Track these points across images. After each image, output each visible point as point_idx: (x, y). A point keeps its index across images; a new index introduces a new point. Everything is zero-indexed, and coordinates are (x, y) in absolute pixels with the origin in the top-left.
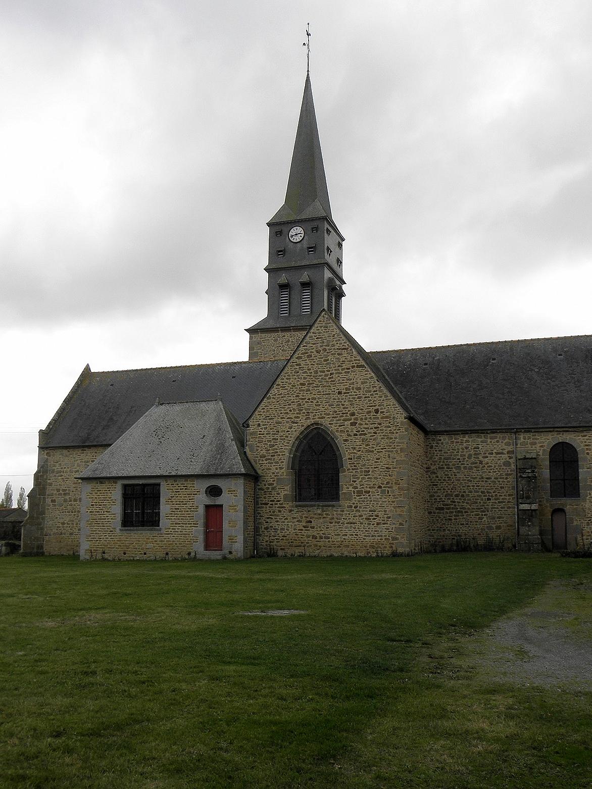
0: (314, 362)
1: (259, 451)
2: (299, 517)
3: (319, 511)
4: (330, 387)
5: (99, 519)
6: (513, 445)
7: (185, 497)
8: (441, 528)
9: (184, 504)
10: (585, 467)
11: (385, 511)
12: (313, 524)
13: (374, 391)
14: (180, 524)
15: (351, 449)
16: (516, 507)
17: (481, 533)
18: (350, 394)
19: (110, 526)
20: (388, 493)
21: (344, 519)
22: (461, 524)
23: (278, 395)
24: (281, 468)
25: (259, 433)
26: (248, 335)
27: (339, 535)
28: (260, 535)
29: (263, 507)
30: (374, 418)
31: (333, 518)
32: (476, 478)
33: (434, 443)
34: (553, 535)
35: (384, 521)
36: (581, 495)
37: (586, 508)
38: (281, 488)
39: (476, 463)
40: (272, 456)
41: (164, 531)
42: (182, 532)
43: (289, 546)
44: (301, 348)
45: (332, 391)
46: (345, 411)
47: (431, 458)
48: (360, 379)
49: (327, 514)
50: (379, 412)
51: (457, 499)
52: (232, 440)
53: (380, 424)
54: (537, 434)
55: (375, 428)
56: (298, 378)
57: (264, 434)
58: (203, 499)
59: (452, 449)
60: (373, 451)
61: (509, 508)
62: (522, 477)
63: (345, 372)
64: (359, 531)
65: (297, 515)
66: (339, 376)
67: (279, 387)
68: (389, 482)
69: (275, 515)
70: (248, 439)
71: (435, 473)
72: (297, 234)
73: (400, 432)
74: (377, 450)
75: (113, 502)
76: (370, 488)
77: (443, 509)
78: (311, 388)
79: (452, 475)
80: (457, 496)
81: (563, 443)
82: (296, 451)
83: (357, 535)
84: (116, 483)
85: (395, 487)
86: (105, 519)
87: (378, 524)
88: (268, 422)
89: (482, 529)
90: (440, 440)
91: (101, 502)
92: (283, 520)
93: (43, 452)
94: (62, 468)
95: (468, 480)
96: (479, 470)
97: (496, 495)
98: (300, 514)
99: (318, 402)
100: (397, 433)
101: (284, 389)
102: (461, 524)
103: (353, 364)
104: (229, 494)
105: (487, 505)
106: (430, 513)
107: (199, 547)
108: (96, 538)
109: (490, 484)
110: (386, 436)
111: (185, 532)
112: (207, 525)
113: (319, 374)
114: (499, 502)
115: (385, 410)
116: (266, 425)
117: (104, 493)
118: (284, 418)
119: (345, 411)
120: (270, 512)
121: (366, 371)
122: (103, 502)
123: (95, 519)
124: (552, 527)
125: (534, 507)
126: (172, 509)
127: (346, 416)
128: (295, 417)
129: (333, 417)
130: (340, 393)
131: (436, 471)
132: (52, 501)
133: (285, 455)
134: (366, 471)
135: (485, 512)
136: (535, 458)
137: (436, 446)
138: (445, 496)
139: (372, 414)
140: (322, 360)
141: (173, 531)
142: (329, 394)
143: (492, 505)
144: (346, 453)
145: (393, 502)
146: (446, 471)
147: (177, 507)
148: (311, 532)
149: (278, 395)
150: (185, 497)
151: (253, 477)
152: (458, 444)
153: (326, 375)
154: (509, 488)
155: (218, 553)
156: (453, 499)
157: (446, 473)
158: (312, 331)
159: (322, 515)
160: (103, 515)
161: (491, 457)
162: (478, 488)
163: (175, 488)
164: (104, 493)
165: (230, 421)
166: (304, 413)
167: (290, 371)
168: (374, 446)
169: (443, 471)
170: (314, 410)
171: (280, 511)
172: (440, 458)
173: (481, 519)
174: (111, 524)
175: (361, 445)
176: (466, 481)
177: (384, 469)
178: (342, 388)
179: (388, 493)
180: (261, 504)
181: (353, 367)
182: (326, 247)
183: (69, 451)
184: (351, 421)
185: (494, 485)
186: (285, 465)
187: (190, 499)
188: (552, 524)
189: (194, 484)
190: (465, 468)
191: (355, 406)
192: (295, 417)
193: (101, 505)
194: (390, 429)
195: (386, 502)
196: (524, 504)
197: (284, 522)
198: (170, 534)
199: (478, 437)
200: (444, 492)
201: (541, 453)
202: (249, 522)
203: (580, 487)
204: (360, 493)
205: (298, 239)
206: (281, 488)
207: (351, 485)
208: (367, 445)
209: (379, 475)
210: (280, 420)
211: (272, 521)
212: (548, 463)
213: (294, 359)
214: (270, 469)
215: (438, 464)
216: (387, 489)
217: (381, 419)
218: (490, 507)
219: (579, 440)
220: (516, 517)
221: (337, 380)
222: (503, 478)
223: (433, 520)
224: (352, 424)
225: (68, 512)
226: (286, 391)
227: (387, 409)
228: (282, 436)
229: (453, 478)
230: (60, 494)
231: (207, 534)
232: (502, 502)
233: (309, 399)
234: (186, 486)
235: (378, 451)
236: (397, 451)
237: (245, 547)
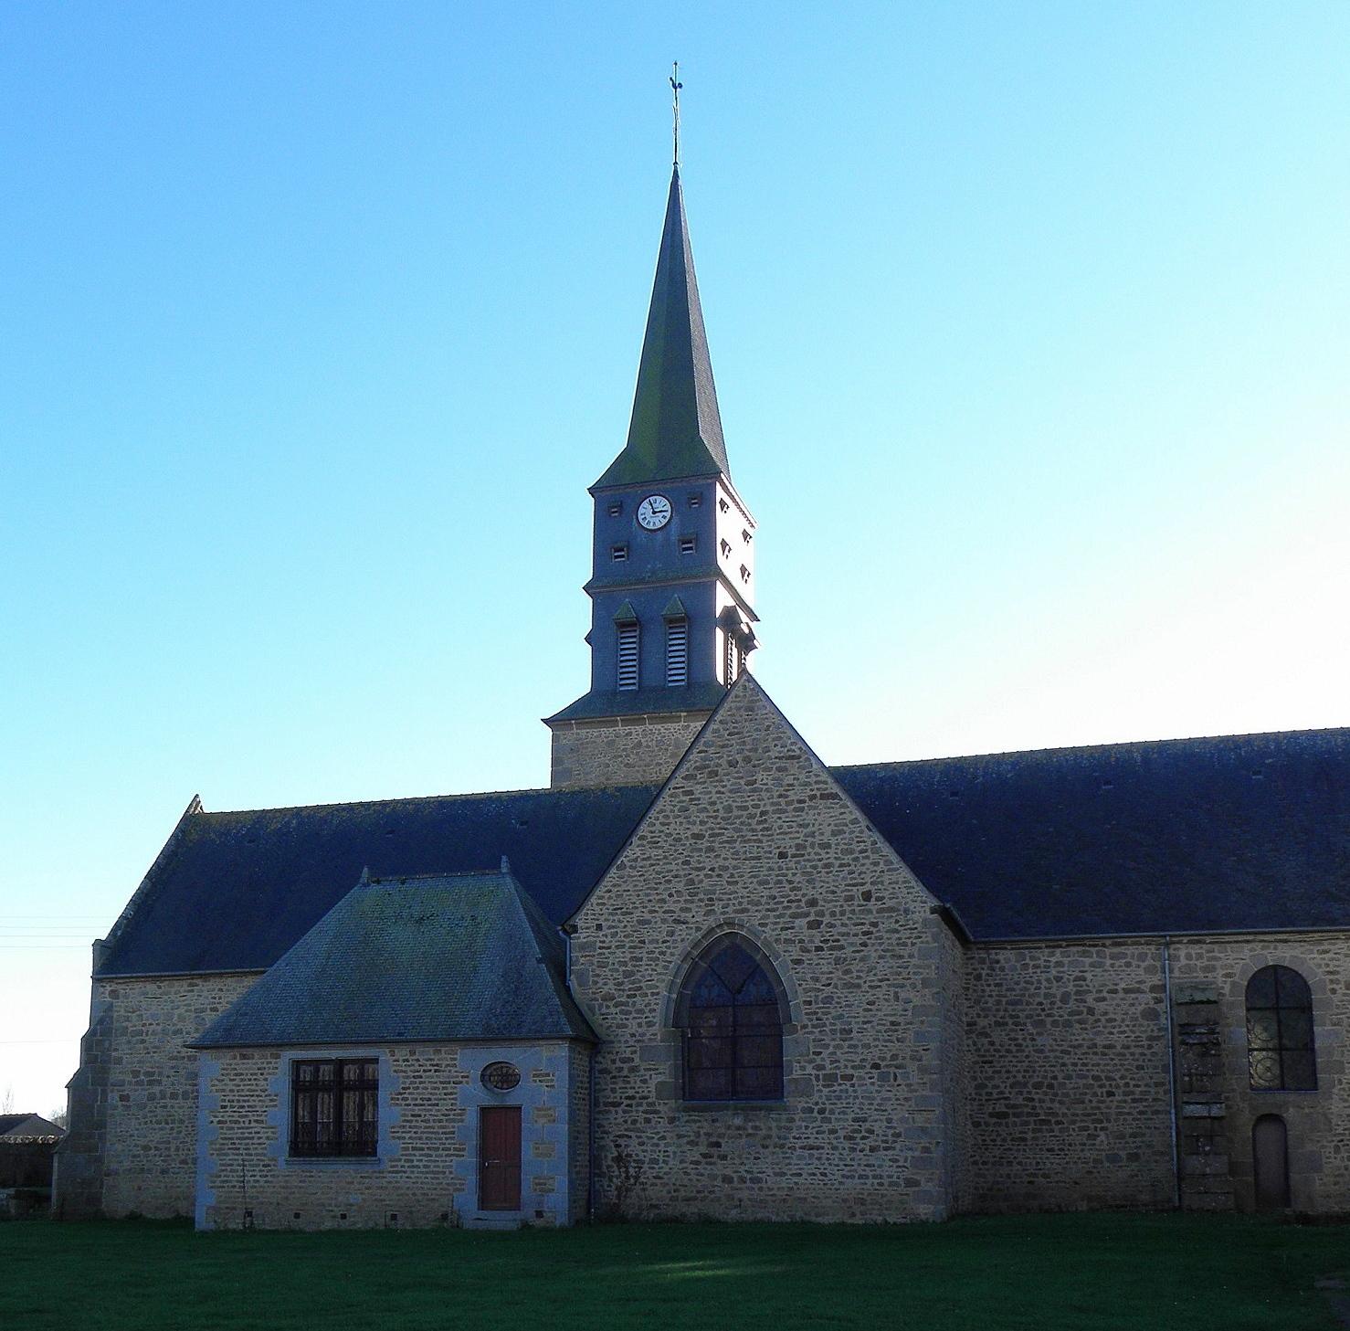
0: (724, 787)
1: (599, 985)
2: (692, 1134)
3: (738, 1121)
4: (761, 842)
5: (238, 1139)
6: (1165, 972)
7: (435, 1089)
8: (1002, 1158)
9: (434, 1105)
10: (1328, 1022)
11: (889, 1121)
12: (724, 1149)
13: (861, 852)
14: (422, 1149)
15: (810, 982)
16: (1173, 1111)
17: (1095, 1170)
18: (807, 857)
19: (265, 1155)
20: (895, 1080)
21: (794, 1138)
22: (1048, 1150)
23: (644, 859)
24: (650, 1024)
25: (599, 944)
26: (548, 732)
27: (785, 1174)
28: (601, 1175)
29: (610, 1111)
30: (862, 912)
31: (769, 1137)
32: (1080, 1046)
33: (983, 969)
34: (1256, 1174)
35: (886, 1142)
36: (1320, 1083)
37: (1332, 1113)
38: (650, 1069)
39: (1080, 1013)
40: (628, 996)
41: (387, 1165)
42: (429, 1167)
43: (670, 1200)
44: (694, 756)
45: (765, 852)
46: (796, 895)
47: (977, 1002)
48: (829, 825)
49: (756, 1128)
50: (873, 899)
51: (1038, 1093)
52: (539, 961)
53: (875, 925)
54: (1216, 947)
55: (865, 933)
56: (689, 823)
57: (609, 948)
58: (476, 1095)
59: (1025, 982)
60: (859, 986)
61: (1157, 1112)
62: (1187, 1044)
63: (796, 810)
64: (830, 1164)
65: (688, 1129)
66: (780, 818)
67: (645, 842)
68: (897, 1055)
69: (638, 1130)
70: (574, 959)
71: (987, 1035)
72: (655, 513)
73: (922, 942)
74: (868, 984)
75: (271, 1100)
76: (853, 1067)
77: (1005, 1115)
78: (716, 845)
79: (1024, 1039)
80: (1038, 1086)
81: (1275, 967)
82: (684, 985)
83: (825, 1175)
84: (278, 1057)
85: (912, 1067)
86: (253, 1138)
87: (872, 1149)
88: (620, 921)
89: (1095, 1161)
90: (998, 962)
91: (244, 1101)
92: (655, 1141)
93: (102, 989)
94: (144, 1025)
95: (1062, 1052)
96: (1086, 1029)
97: (1127, 1085)
98: (695, 1126)
99: (732, 876)
100: (913, 944)
101: (656, 848)
102: (1048, 1150)
103: (812, 790)
104: (536, 1081)
105: (1107, 1108)
106: (976, 1125)
107: (467, 1201)
108: (231, 1181)
109: (1112, 1059)
110: (887, 951)
111: (435, 1167)
112: (484, 1152)
113: (736, 813)
114: (1134, 1101)
115: (886, 894)
116: (614, 927)
117: (250, 1080)
118: (657, 912)
119: (796, 895)
120: (626, 1122)
121: (842, 807)
122: (248, 1101)
123: (230, 1139)
124: (1255, 1156)
125: (1215, 1111)
126: (405, 1115)
127: (798, 907)
128: (682, 910)
129: (768, 910)
130: (782, 855)
131: (988, 1030)
132: (122, 1098)
133: (658, 994)
134: (844, 1029)
135: (1102, 1122)
136: (1215, 1002)
137: (988, 974)
138: (1011, 1087)
139: (856, 903)
140: (742, 782)
141: (407, 1164)
142: (759, 858)
143: (1117, 1107)
144: (800, 990)
145: (906, 1099)
146: (1012, 1030)
147: (416, 1112)
148: (720, 1169)
149: (644, 859)
150: (435, 1089)
151: (589, 1041)
152: (1039, 971)
153: (751, 816)
154: (1156, 1068)
155: (511, 1215)
156: (1029, 1093)
157: (1013, 1035)
158: (718, 717)
159: (745, 1129)
160: (248, 1128)
161: (1113, 999)
162: (1085, 1068)
163: (412, 1068)
164: (250, 1080)
165: (527, 915)
166: (701, 900)
167: (668, 808)
168: (861, 974)
169: (1005, 1030)
170: (726, 893)
171: (648, 1121)
172: (999, 1003)
173: (1092, 1137)
174: (265, 1148)
175: (831, 973)
176: (1058, 1054)
177: (884, 1025)
178: (788, 844)
179: (895, 1080)
180: (606, 1104)
181: (813, 797)
182: (719, 541)
183: (160, 987)
184: (808, 919)
185: (1122, 1062)
186: (658, 1018)
187: (445, 1094)
188: (1254, 1149)
189: (455, 1059)
190: (1055, 1023)
191: (818, 885)
192: (682, 910)
193: (243, 1107)
194: (897, 936)
195: (890, 1099)
196: (1192, 1103)
197: (657, 1145)
198: (401, 1172)
199: (1085, 954)
200: (1008, 1078)
201: (1227, 990)
202: (580, 1144)
203: (1318, 1066)
204: (831, 1079)
205: (659, 522)
206: (650, 1069)
207: (810, 1062)
208: (847, 972)
209: (875, 1040)
210: (647, 916)
211: (629, 1141)
212: (1243, 1012)
213: (678, 781)
214: (626, 1026)
215: (995, 1016)
216: (892, 1070)
217: (878, 913)
218: (1113, 1111)
219: (1312, 961)
220: (1174, 1134)
221: (775, 826)
222: (1142, 1046)
223: (984, 1140)
224: (811, 925)
225: (158, 1122)
226: (661, 851)
227: (891, 891)
228: (653, 952)
229: (1027, 1046)
230: (139, 1083)
231: (483, 1171)
232: (1141, 1100)
233: (712, 870)
234: (437, 1065)
235: (873, 984)
236: (914, 986)
237: (573, 1202)
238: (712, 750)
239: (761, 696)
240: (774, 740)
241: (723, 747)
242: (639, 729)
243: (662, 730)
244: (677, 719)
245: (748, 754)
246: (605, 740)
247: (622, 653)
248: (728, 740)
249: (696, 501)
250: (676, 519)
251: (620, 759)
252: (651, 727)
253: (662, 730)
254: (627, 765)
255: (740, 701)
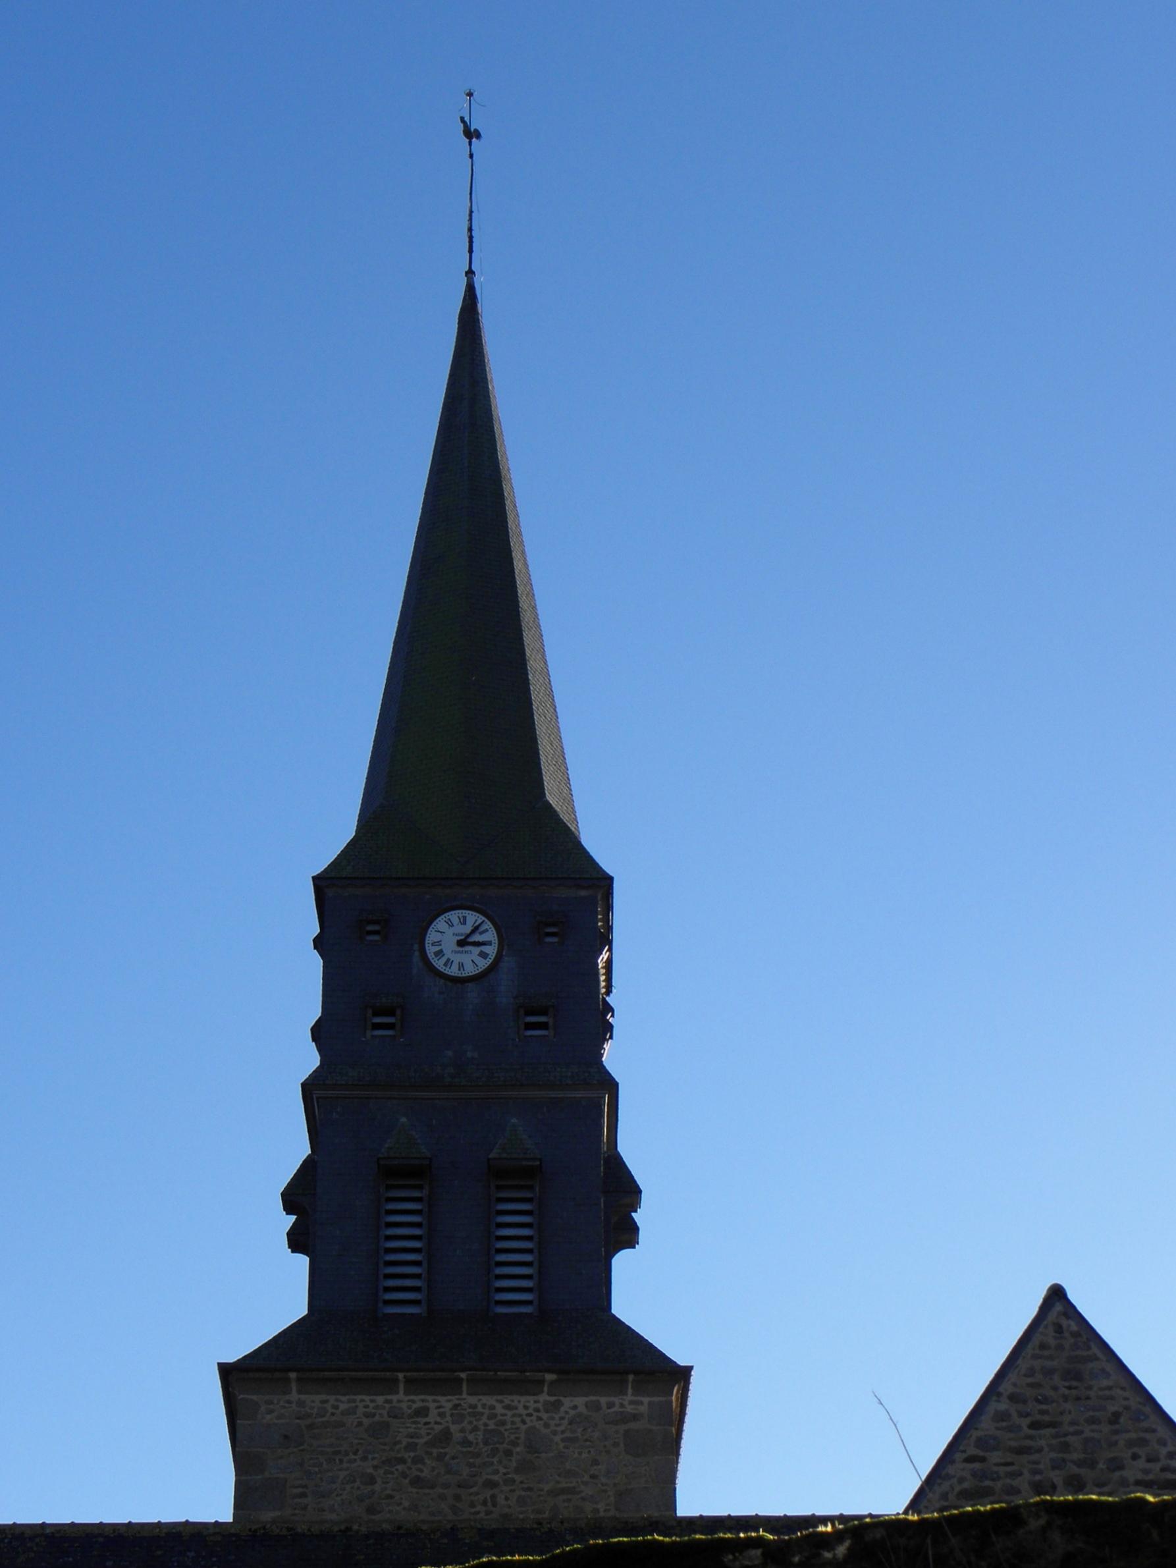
205: (471, 963)
238: (995, 1457)
239: (1095, 1350)
240: (1130, 1444)
241: (1020, 1451)
242: (447, 1402)
243: (499, 1409)
244: (531, 1387)
245: (1075, 1470)
246: (366, 1421)
247: (391, 1232)
248: (1031, 1437)
249: (377, 928)
250: (508, 962)
251: (400, 1467)
252: (473, 1400)
253: (499, 1409)
254: (417, 1482)
255: (1051, 1358)
